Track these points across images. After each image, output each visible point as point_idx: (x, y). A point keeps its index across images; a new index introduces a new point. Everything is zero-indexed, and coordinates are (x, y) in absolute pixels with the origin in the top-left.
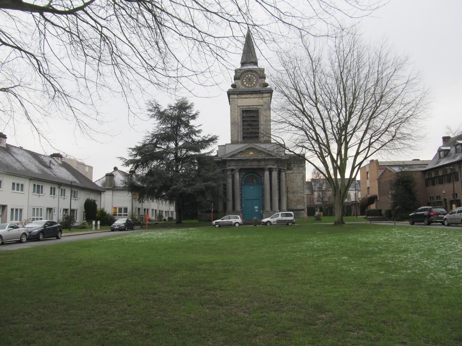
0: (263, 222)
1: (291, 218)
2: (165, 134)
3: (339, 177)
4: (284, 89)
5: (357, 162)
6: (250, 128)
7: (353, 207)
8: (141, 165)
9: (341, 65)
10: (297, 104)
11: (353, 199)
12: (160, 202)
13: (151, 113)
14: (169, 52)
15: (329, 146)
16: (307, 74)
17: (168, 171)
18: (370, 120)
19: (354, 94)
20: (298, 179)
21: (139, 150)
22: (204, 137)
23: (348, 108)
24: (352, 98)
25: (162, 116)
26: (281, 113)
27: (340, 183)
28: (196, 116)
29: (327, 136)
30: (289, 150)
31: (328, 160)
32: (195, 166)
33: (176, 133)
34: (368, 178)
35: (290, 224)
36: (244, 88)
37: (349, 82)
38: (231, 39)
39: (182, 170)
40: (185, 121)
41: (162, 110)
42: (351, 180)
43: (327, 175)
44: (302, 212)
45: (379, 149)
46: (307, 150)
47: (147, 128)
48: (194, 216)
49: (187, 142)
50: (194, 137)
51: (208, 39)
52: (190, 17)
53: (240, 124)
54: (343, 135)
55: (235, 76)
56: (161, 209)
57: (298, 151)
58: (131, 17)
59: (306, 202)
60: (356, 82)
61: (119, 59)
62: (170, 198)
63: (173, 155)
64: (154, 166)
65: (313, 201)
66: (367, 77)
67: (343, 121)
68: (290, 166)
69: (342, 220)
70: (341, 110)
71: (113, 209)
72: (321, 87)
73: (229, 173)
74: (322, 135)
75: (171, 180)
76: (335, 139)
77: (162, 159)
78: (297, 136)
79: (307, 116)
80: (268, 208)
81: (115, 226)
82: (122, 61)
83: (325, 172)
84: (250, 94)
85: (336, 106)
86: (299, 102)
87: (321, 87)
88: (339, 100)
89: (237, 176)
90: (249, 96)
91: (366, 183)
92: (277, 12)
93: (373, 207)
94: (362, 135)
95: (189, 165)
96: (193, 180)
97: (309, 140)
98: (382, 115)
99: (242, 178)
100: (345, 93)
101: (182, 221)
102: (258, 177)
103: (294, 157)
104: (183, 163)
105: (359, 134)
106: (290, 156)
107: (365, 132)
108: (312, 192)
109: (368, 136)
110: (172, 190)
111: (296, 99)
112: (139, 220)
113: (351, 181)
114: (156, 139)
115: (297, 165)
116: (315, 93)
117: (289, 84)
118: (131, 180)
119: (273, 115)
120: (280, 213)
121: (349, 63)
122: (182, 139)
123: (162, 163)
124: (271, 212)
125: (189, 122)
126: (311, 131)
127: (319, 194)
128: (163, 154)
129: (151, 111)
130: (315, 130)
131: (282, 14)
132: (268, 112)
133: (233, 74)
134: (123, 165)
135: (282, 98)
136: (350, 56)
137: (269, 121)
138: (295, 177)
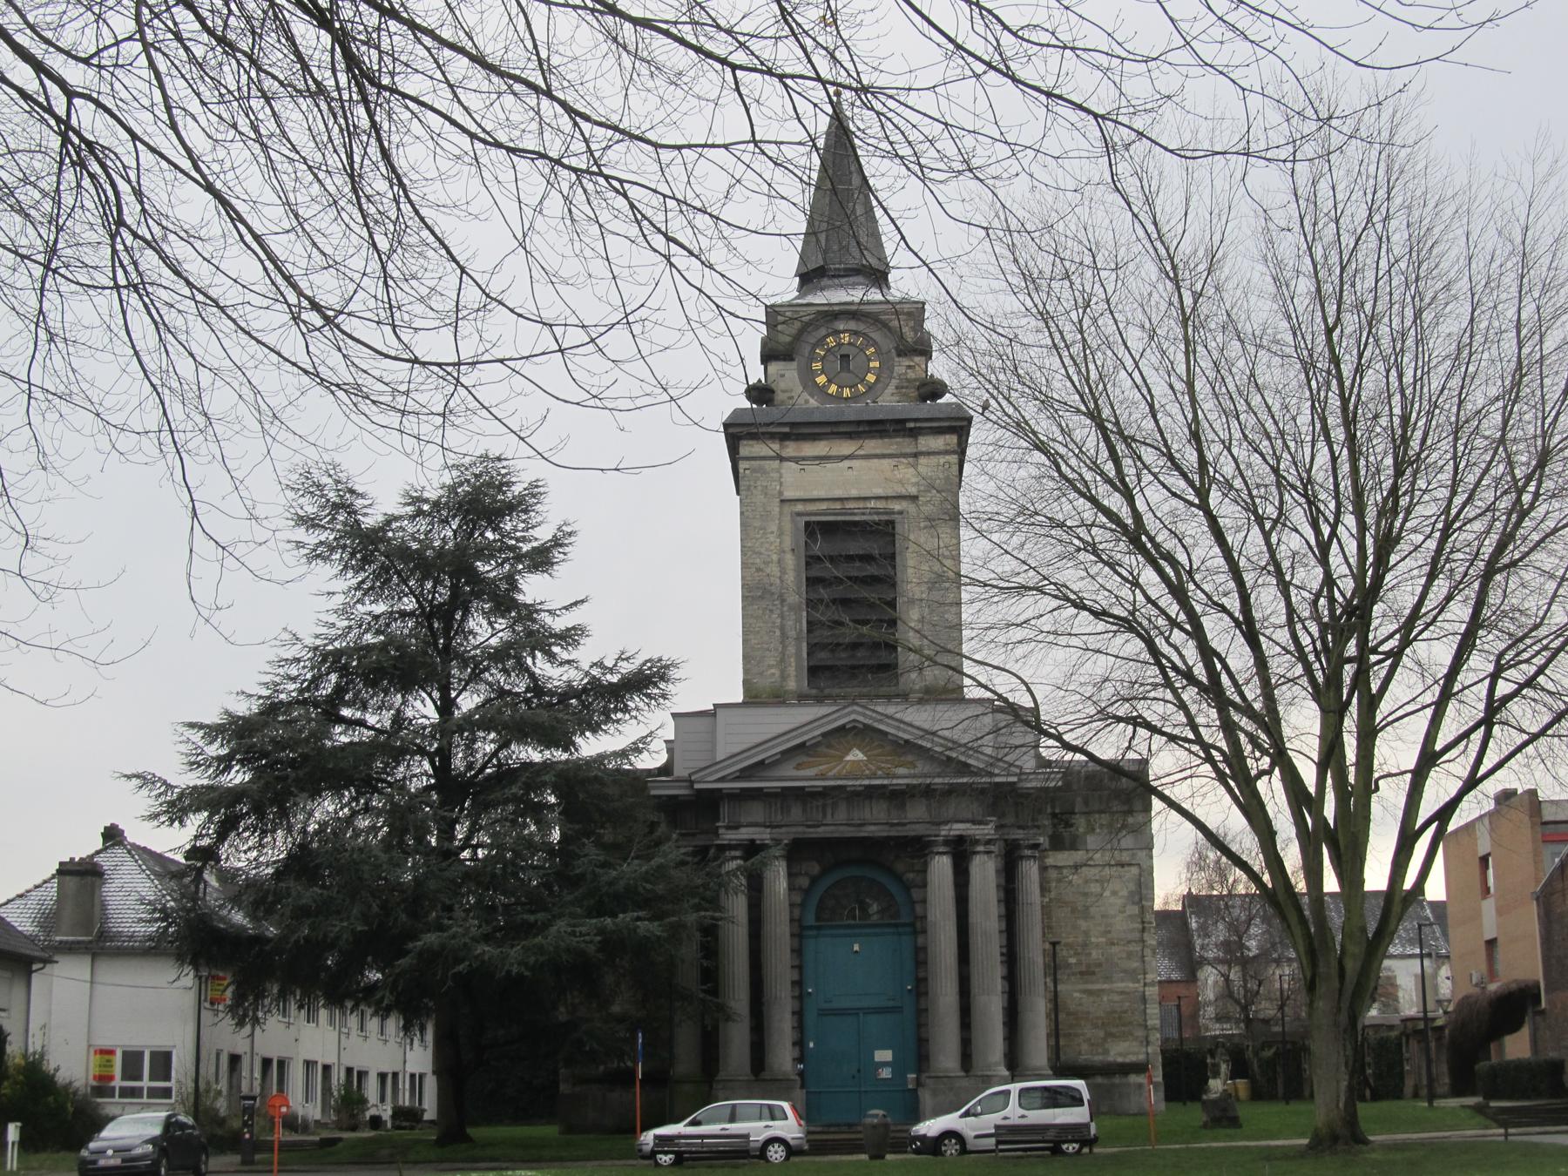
0: (923, 1138)
1: (1076, 1115)
2: (383, 647)
3: (1331, 883)
4: (1030, 410)
5: (1429, 805)
6: (846, 619)
7: (1413, 1050)
8: (251, 820)
9: (1327, 288)
10: (1102, 491)
11: (1409, 1004)
12: (353, 1021)
13: (312, 538)
14: (414, 223)
15: (1277, 720)
16: (1152, 334)
17: (396, 853)
18: (1487, 577)
19: (1400, 443)
20: (1113, 900)
21: (241, 735)
22: (599, 664)
23: (1370, 519)
24: (1389, 461)
25: (369, 549)
26: (1016, 541)
27: (1336, 918)
28: (557, 555)
29: (1261, 663)
30: (1058, 738)
31: (1272, 791)
32: (544, 826)
33: (447, 646)
34: (1487, 890)
35: (1071, 1148)
36: (813, 403)
37: (1372, 381)
38: (746, 158)
39: (475, 845)
40: (494, 580)
41: (369, 521)
42: (1400, 901)
43: (1266, 878)
44: (1134, 1078)
45: (1543, 732)
46: (1158, 740)
47: (286, 614)
48: (535, 1103)
49: (502, 693)
50: (540, 665)
51: (625, 160)
52: (530, 45)
53: (796, 597)
54: (1350, 660)
55: (765, 343)
56: (357, 1065)
57: (1109, 745)
58: (222, 40)
59: (1154, 1021)
60: (1408, 378)
61: (149, 259)
62: (406, 1004)
63: (427, 765)
64: (323, 825)
65: (1195, 1016)
66: (1463, 353)
67: (1348, 585)
68: (1068, 825)
69: (1351, 1120)
70: (1334, 528)
71: (95, 1060)
72: (1228, 404)
73: (733, 865)
74: (1239, 658)
75: (416, 898)
76: (1304, 681)
77: (368, 785)
78: (1100, 665)
79: (1156, 557)
80: (947, 1058)
81: (102, 1152)
82: (167, 272)
83: (1257, 862)
84: (850, 436)
85: (1310, 503)
86: (1109, 481)
87: (1228, 404)
88: (1321, 474)
89: (778, 880)
90: (847, 447)
91: (1476, 916)
92: (980, 28)
93: (1517, 1046)
94: (1448, 660)
95: (514, 822)
96: (535, 901)
97: (1168, 684)
98: (1551, 553)
99: (807, 892)
100: (1351, 438)
101: (471, 1131)
102: (893, 887)
103: (1090, 777)
104: (482, 807)
105: (1435, 651)
106: (1068, 770)
107: (1466, 645)
108: (1191, 966)
109: (1480, 664)
110: (420, 954)
111: (1095, 467)
112: (236, 1124)
113: (1396, 908)
114: (333, 677)
115: (1105, 819)
116: (1195, 437)
117: (1056, 384)
118: (194, 899)
119: (974, 551)
120: (1015, 1088)
121: (1370, 282)
122: (475, 677)
123: (367, 809)
124: (965, 1083)
125: (514, 587)
126: (1177, 636)
127: (1227, 979)
128: (371, 757)
129: (309, 522)
130: (1198, 633)
131: (1007, 39)
132: (945, 531)
133: (753, 339)
134: (155, 816)
135: (1020, 462)
136: (1374, 244)
137: (949, 580)
138: (1095, 888)
